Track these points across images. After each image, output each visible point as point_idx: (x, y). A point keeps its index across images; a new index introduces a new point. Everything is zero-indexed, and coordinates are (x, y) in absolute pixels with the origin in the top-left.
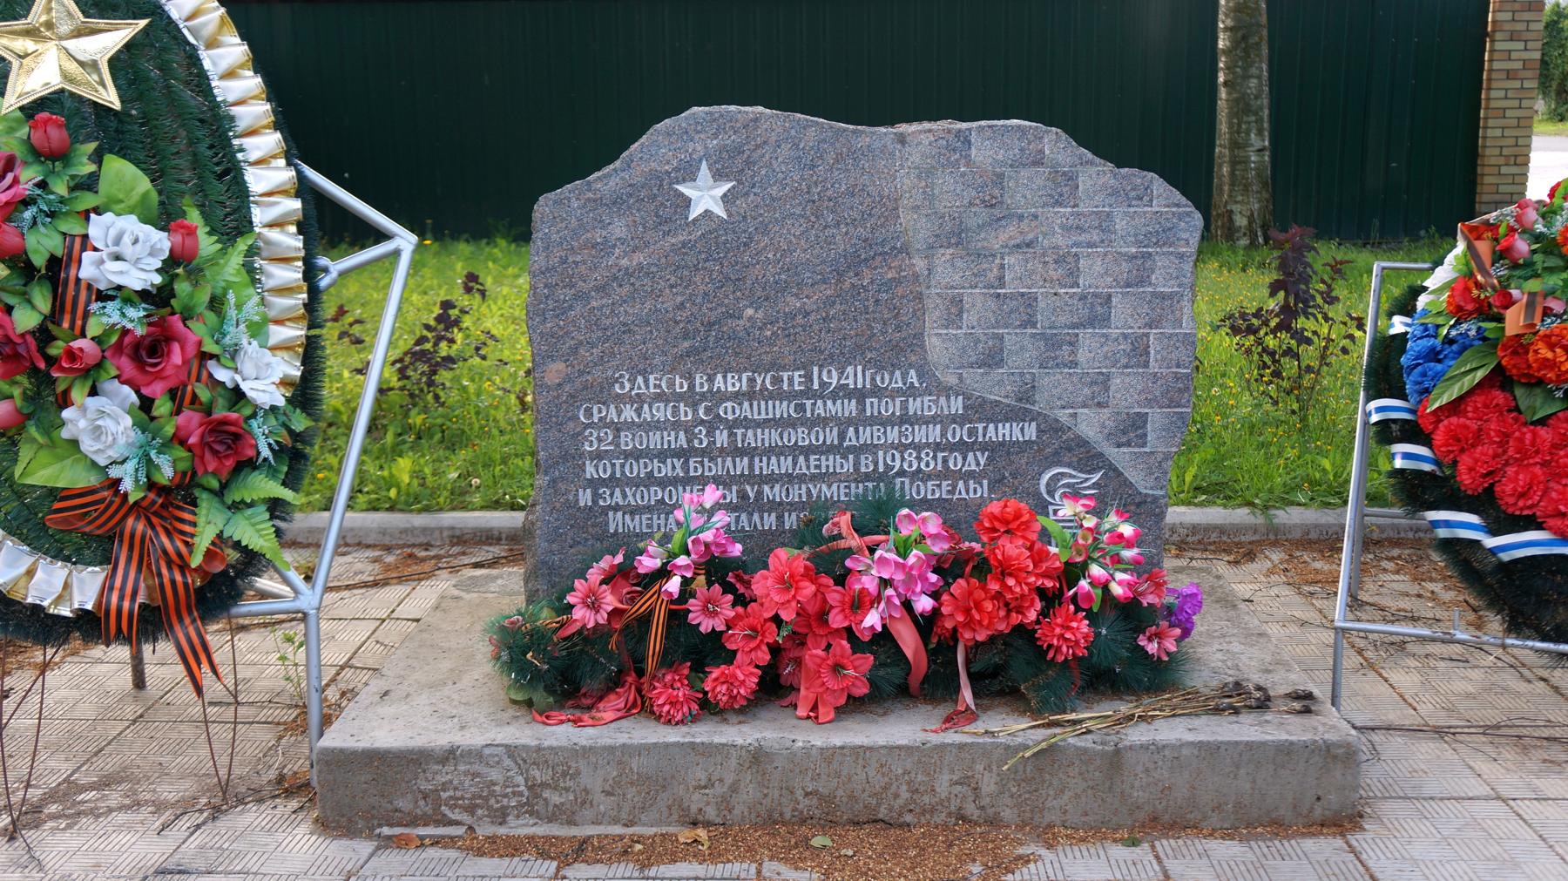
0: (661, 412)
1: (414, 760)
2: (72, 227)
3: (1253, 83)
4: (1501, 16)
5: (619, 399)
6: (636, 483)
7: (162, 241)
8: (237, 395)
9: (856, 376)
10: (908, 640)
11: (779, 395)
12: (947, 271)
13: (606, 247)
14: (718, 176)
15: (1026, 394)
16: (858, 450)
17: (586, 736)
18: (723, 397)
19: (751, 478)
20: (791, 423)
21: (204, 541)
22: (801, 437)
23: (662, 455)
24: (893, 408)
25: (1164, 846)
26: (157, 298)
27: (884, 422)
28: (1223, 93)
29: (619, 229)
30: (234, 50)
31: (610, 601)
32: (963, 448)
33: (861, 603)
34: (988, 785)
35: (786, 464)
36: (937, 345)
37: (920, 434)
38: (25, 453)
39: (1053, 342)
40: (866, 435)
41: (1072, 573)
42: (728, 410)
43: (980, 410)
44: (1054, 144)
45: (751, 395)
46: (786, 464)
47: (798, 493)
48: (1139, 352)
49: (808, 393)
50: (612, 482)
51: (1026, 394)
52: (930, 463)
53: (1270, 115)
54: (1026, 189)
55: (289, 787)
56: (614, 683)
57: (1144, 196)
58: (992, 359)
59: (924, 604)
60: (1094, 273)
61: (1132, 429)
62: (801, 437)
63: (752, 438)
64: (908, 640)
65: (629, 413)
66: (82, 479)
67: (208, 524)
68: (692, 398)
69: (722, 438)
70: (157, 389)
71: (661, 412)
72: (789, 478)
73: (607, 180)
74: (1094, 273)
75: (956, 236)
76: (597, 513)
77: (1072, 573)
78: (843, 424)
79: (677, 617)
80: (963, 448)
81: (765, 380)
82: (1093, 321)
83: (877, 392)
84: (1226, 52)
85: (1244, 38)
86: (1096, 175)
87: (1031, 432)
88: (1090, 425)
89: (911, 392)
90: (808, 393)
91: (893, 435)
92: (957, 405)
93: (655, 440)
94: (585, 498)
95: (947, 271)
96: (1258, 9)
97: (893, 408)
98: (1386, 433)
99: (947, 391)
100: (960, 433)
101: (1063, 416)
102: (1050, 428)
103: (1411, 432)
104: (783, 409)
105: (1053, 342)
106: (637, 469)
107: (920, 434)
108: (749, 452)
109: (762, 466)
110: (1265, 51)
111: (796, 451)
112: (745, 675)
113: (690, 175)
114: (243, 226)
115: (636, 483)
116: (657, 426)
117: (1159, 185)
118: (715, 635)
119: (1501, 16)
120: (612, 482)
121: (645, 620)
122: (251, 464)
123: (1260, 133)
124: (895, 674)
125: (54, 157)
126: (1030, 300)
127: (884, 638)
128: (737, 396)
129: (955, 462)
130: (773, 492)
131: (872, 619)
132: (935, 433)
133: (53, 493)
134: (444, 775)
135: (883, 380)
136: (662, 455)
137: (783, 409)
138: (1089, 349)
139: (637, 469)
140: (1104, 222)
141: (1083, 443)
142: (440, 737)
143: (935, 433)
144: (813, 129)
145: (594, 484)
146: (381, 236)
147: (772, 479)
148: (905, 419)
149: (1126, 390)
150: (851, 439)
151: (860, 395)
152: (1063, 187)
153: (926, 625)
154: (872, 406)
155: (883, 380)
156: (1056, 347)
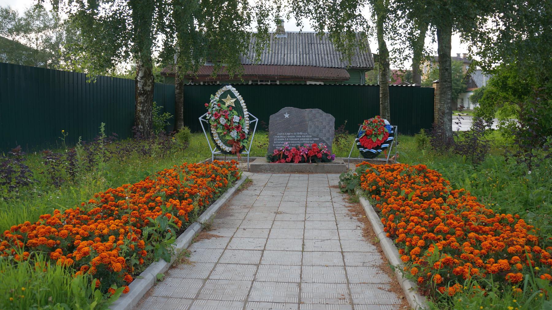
0: (282, 137)
1: (259, 165)
2: (232, 117)
3: (386, 104)
4: (437, 92)
5: (278, 135)
6: (279, 144)
7: (239, 118)
8: (244, 132)
9: (301, 133)
10: (305, 156)
11: (294, 135)
12: (310, 123)
13: (277, 120)
14: (288, 114)
15: (318, 135)
16: (301, 141)
17: (275, 164)
18: (288, 135)
19: (291, 143)
20: (294, 138)
21: (241, 145)
22: (295, 139)
23: (282, 141)
24: (305, 137)
25: (328, 174)
26: (239, 123)
27: (304, 138)
28: (381, 105)
29: (278, 119)
30: (243, 101)
31: (277, 152)
32: (311, 141)
33: (300, 153)
34: (312, 169)
35: (294, 142)
36: (309, 130)
37: (307, 139)
38: (226, 136)
39: (320, 130)
40: (302, 139)
41: (321, 150)
42: (288, 137)
43: (313, 137)
44: (320, 111)
45: (291, 135)
46: (294, 142)
47: (295, 145)
48: (329, 131)
49: (296, 135)
50: (277, 144)
51: (318, 135)
52: (308, 142)
53: (390, 110)
54: (318, 115)
55: (169, 269)
56: (277, 160)
57: (329, 116)
58: (314, 132)
59: (306, 153)
60: (324, 123)
61: (328, 139)
62: (295, 139)
63: (291, 139)
64: (305, 156)
65: (279, 137)
66: (231, 139)
67: (241, 144)
68: (285, 135)
69: (288, 139)
70: (238, 131)
71: (282, 137)
72: (294, 143)
73: (277, 114)
74: (324, 123)
75: (311, 120)
76: (275, 147)
77: (321, 150)
78: (300, 138)
79: (284, 154)
80: (311, 141)
81: (292, 134)
82: (324, 128)
83: (303, 135)
84: (381, 98)
85: (384, 95)
86: (325, 114)
87: (318, 139)
88: (324, 139)
89: (306, 135)
90: (296, 135)
91: (305, 139)
92: (311, 136)
93: (281, 139)
94: (274, 145)
95: (310, 123)
96: (387, 90)
97: (305, 137)
98: (357, 141)
99: (310, 135)
100: (311, 139)
101: (321, 138)
102: (320, 139)
103: (359, 141)
104: (294, 137)
105: (320, 130)
106: (279, 142)
107: (307, 139)
108: (290, 141)
109: (292, 142)
110: (389, 98)
111: (295, 141)
112: (290, 159)
113: (285, 114)
114: (244, 118)
115: (279, 144)
116: (281, 138)
117: (331, 115)
118: (287, 156)
119: (437, 92)
120: (277, 144)
121: (281, 154)
122: (245, 139)
123: (388, 113)
124: (303, 159)
125: (231, 111)
126: (318, 126)
127: (303, 156)
128: (289, 135)
129: (311, 142)
130: (293, 145)
131: (302, 154)
132: (309, 139)
133: (228, 140)
134: (262, 167)
135: (304, 134)
136: (282, 141)
137: (294, 137)
138: (324, 131)
139: (279, 142)
140: (325, 119)
141: (323, 140)
142: (262, 164)
143: (309, 139)
144: (297, 109)
145: (275, 144)
146: (255, 119)
147: (293, 144)
148: (306, 138)
149: (328, 135)
150: (300, 140)
151: (301, 135)
152: (321, 115)
153: (307, 155)
154: (303, 136)
155: (304, 134)
156: (321, 131)
